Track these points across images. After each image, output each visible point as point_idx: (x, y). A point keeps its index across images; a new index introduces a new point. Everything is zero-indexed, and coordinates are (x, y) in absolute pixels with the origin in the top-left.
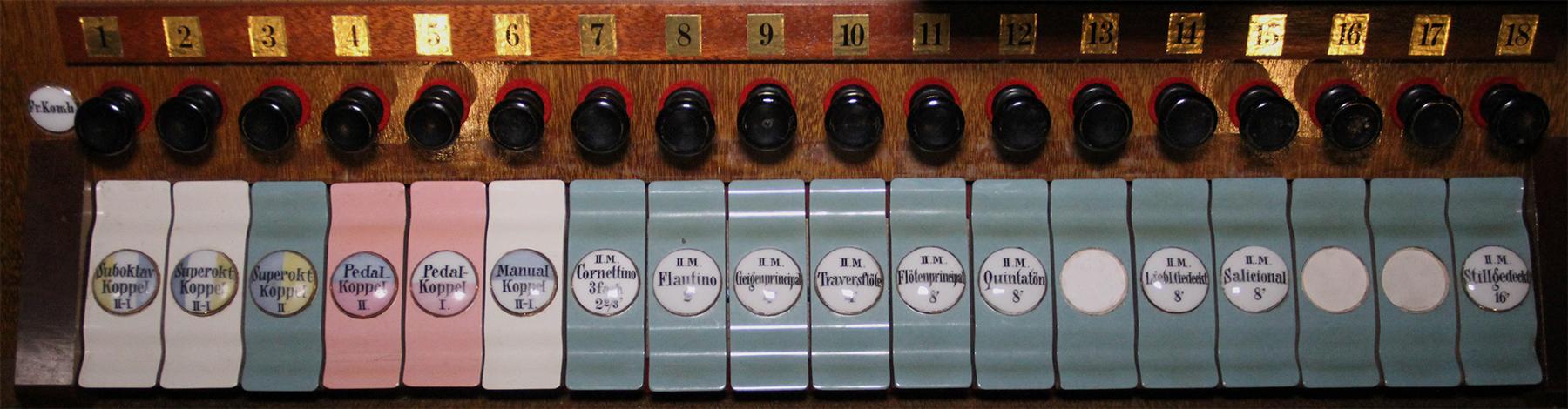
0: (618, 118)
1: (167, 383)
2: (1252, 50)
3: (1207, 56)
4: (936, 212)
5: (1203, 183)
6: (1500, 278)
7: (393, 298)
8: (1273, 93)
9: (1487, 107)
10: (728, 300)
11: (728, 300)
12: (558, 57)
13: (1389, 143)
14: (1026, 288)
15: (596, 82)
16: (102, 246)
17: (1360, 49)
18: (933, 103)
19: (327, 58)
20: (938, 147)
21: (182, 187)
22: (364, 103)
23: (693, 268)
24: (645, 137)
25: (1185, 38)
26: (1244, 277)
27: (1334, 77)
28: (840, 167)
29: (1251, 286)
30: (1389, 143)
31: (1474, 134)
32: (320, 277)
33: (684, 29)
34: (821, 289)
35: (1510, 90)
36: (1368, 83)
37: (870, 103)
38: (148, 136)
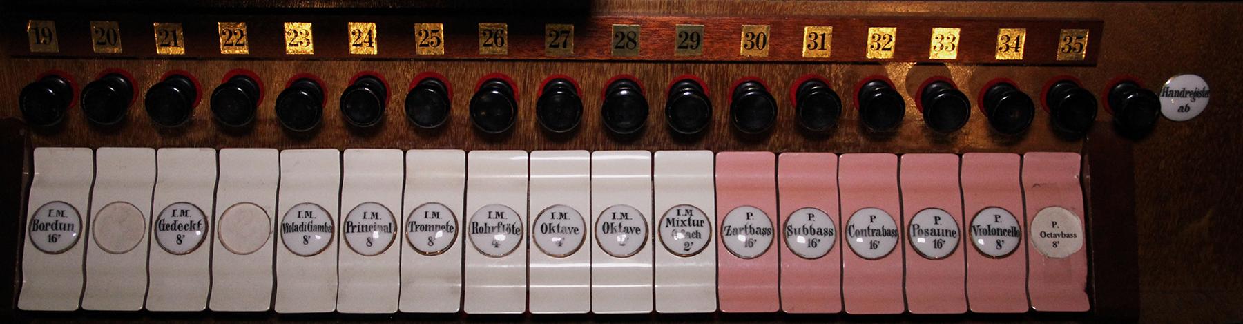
0: (639, 102)
1: (214, 307)
2: (935, 54)
3: (899, 57)
4: (691, 176)
5: (463, 153)
6: (1063, 230)
7: (518, 246)
8: (887, 86)
9: (1052, 99)
10: (528, 247)
11: (528, 247)
12: (716, 58)
13: (976, 127)
14: (759, 237)
15: (415, 79)
16: (37, 198)
17: (1019, 56)
18: (624, 93)
19: (797, 59)
20: (631, 128)
21: (288, 154)
22: (563, 88)
23: (374, 220)
24: (527, 117)
25: (107, 44)
26: (989, 231)
27: (753, 74)
28: (800, 140)
29: (993, 239)
30: (976, 127)
31: (1041, 119)
32: (721, 231)
33: (631, 36)
34: (726, 238)
35: (1070, 83)
36: (960, 77)
37: (508, 92)
38: (76, 114)
